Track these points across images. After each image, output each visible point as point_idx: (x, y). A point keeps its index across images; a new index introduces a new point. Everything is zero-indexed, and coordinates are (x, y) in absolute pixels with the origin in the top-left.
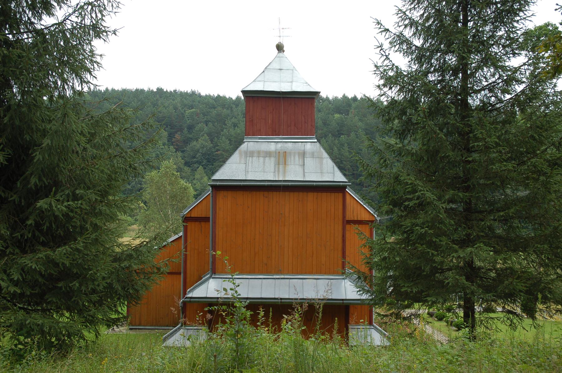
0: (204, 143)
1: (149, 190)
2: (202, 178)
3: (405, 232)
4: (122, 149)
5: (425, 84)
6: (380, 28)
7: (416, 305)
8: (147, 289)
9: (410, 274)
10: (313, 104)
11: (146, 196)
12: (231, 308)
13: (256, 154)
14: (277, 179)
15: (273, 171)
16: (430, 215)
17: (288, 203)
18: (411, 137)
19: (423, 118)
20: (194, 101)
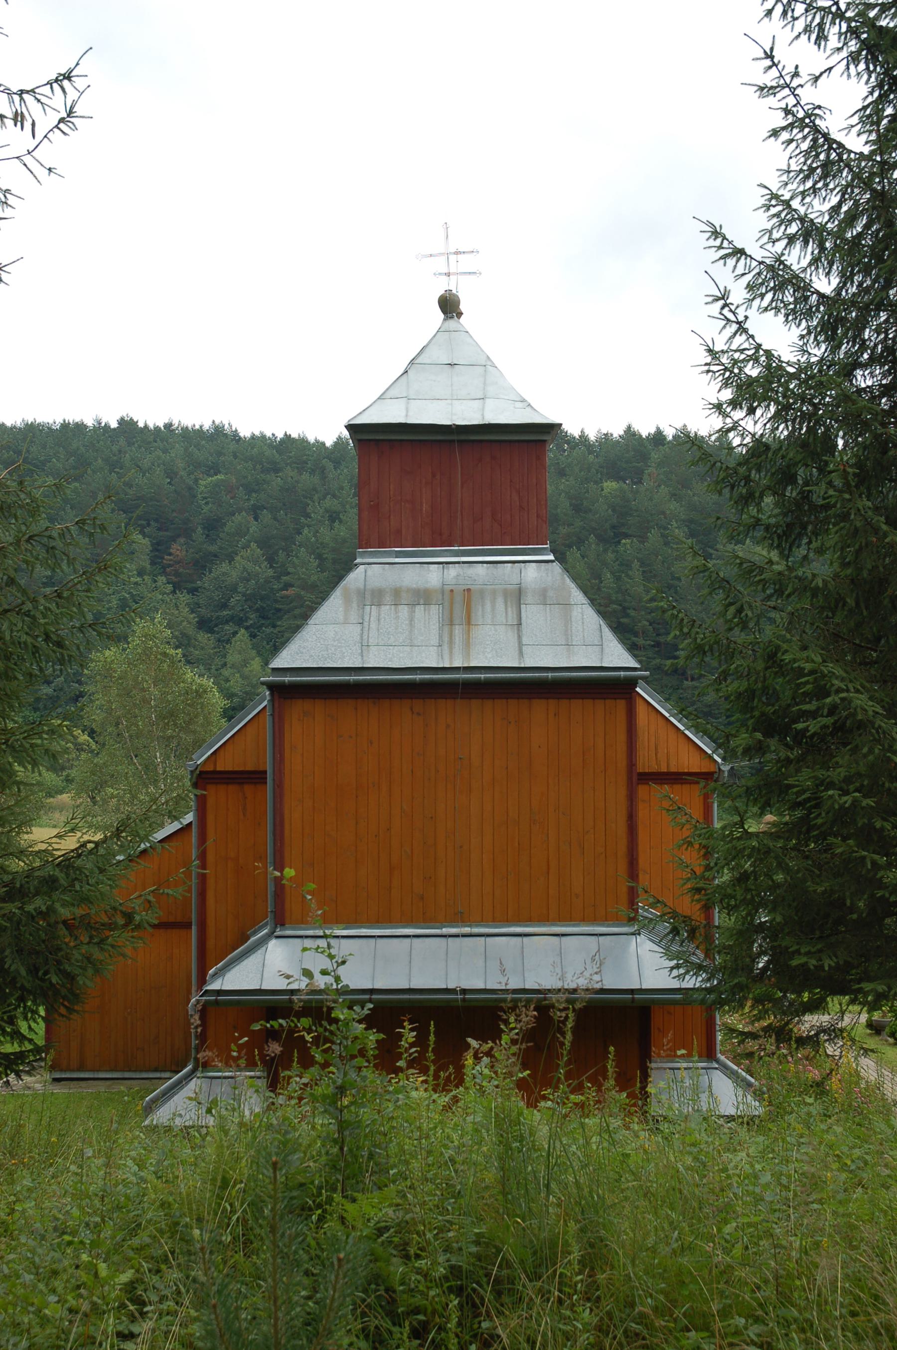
0: (249, 566)
1: (100, 699)
2: (245, 663)
3: (799, 804)
4: (24, 592)
5: (844, 398)
6: (720, 247)
7: (834, 1003)
8: (97, 971)
9: (811, 918)
10: (540, 457)
11: (95, 715)
12: (325, 1023)
13: (388, 598)
14: (447, 665)
15: (435, 640)
16: (865, 756)
17: (479, 723)
18: (810, 542)
19: (840, 491)
20: (220, 454)
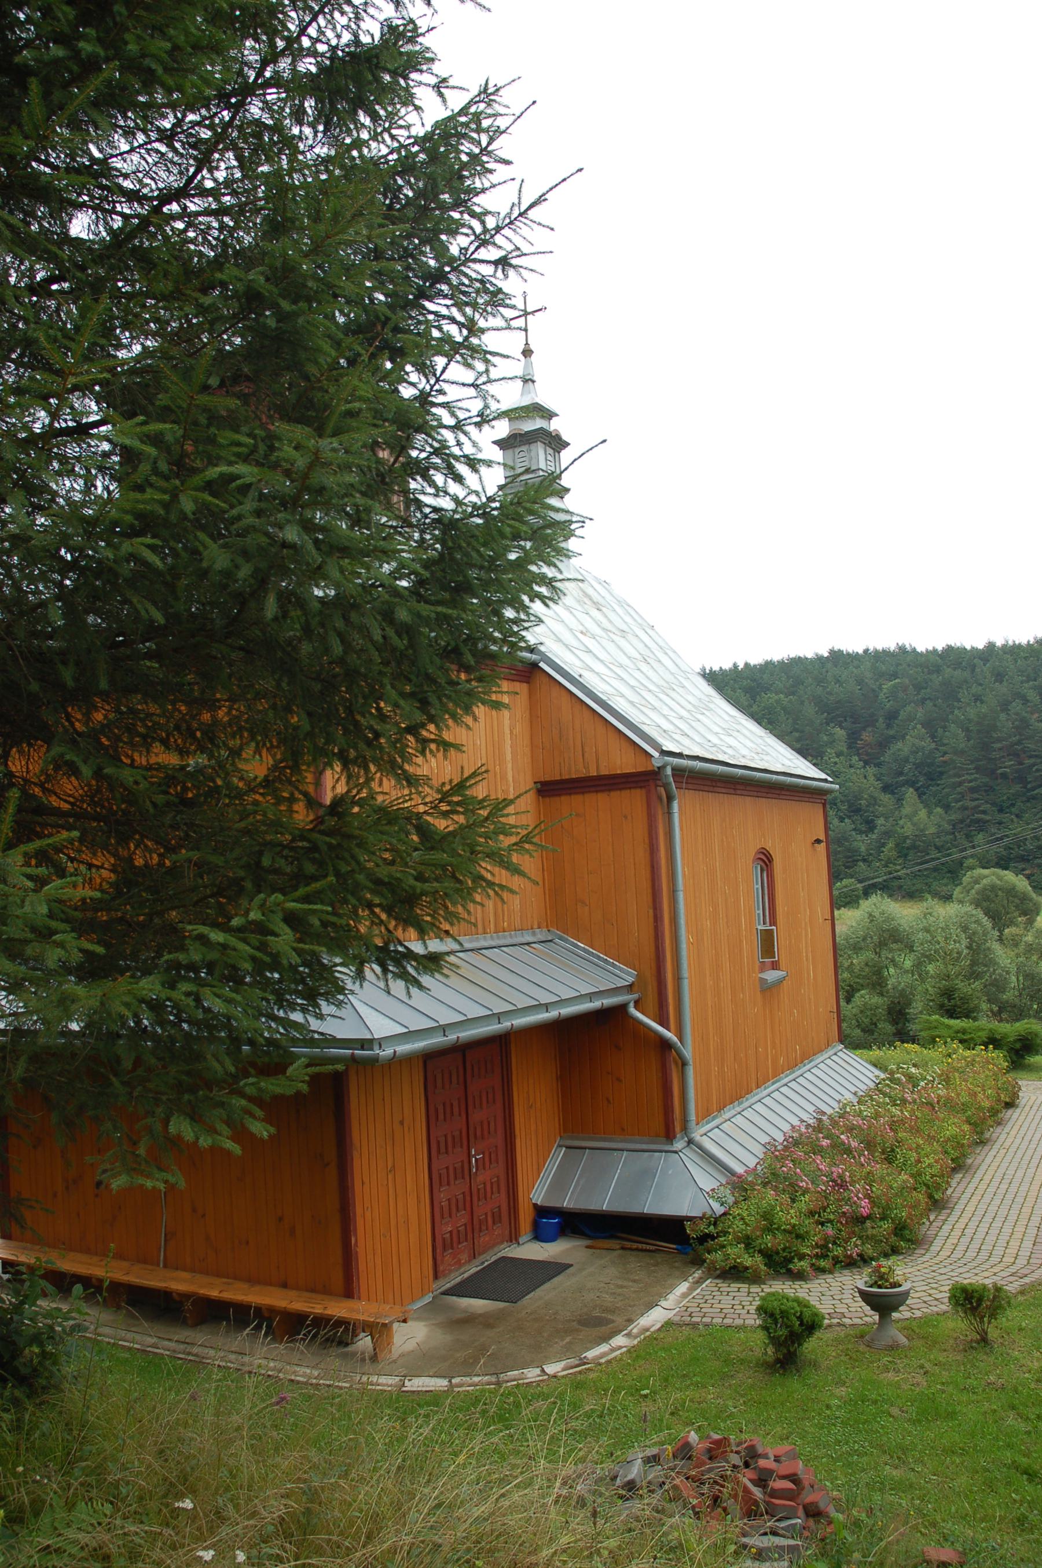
2: (915, 813)
